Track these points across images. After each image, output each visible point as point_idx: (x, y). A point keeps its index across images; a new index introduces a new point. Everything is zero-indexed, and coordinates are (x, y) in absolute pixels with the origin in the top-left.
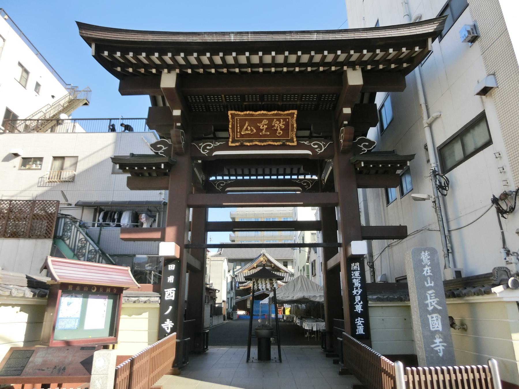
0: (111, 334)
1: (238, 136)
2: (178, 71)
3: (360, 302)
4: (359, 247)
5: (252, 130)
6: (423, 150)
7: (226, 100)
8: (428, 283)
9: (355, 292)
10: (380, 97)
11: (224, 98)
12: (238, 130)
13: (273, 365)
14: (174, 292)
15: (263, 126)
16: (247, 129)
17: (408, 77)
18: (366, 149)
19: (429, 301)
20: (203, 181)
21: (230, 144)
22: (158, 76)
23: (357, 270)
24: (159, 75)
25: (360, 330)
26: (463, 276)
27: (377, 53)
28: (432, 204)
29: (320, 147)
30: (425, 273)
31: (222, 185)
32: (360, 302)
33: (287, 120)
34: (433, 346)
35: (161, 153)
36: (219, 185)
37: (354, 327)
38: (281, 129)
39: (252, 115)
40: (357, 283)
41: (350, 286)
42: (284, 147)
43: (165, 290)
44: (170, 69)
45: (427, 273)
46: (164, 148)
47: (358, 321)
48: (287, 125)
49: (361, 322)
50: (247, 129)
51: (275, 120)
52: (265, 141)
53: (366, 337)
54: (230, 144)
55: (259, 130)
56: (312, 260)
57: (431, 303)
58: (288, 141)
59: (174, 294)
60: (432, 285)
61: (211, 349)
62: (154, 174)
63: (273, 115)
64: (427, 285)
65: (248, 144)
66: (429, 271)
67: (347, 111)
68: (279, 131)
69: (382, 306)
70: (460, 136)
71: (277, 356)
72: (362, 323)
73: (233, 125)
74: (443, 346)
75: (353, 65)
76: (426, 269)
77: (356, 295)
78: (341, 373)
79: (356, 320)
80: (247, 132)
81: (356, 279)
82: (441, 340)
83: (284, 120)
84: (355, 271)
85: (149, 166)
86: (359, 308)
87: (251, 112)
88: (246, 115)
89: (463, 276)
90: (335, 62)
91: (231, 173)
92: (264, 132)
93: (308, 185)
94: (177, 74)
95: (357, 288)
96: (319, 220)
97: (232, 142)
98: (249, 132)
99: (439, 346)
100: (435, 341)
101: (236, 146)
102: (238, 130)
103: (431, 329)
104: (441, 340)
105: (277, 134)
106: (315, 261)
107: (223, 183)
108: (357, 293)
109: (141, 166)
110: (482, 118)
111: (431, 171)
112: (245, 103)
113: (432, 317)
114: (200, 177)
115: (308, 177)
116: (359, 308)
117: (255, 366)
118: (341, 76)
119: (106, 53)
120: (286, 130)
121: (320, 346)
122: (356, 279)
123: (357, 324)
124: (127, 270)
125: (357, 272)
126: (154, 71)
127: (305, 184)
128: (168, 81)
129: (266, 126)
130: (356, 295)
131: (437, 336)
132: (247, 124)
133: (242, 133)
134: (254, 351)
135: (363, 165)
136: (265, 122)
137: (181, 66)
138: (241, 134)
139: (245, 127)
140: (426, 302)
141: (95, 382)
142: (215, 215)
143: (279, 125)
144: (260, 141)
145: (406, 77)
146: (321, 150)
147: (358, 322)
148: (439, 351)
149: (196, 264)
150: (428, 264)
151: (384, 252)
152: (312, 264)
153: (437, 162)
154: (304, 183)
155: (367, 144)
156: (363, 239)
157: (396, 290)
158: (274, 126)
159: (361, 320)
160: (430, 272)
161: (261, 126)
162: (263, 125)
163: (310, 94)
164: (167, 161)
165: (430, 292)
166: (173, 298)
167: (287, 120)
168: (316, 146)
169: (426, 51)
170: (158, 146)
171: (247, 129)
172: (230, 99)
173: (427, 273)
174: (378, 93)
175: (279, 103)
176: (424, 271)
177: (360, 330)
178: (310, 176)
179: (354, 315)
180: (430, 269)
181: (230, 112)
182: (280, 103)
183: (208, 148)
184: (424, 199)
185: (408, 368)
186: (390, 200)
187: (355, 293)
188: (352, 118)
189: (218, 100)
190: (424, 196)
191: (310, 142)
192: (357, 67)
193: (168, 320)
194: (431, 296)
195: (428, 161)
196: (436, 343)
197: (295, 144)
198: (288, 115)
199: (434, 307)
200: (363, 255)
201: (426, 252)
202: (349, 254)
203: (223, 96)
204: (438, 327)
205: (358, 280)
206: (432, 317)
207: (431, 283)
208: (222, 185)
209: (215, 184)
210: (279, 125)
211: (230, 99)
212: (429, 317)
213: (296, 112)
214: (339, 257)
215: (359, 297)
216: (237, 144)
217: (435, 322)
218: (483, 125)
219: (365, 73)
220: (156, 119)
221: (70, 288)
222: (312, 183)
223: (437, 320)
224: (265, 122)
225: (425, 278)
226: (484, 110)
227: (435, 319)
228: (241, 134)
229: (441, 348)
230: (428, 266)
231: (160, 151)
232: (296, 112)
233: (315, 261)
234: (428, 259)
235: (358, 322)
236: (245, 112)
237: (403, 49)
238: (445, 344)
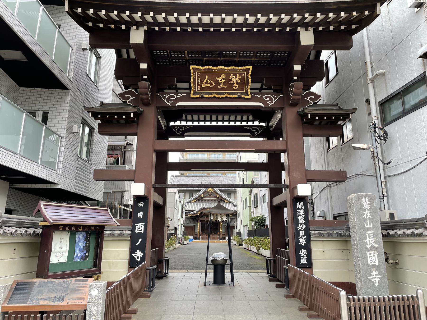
0: (95, 266)
1: (199, 89)
2: (146, 28)
3: (303, 236)
4: (303, 190)
5: (211, 84)
6: (365, 104)
7: (188, 55)
8: (367, 225)
9: (299, 227)
10: (325, 55)
11: (186, 54)
12: (199, 83)
13: (227, 288)
14: (143, 226)
15: (221, 80)
16: (206, 83)
17: (355, 37)
18: (312, 102)
19: (368, 240)
20: (164, 126)
21: (192, 96)
22: (127, 32)
23: (302, 209)
24: (128, 31)
25: (304, 260)
26: (396, 218)
27: (330, 16)
28: (371, 155)
29: (271, 100)
30: (365, 215)
31: (181, 130)
32: (303, 236)
33: (243, 75)
34: (370, 278)
35: (129, 102)
36: (178, 130)
37: (298, 257)
38: (237, 83)
39: (211, 70)
40: (301, 220)
41: (296, 222)
42: (239, 99)
43: (136, 225)
44: (139, 25)
45: (367, 216)
46: (131, 98)
47: (302, 252)
48: (242, 79)
49: (304, 253)
50: (207, 83)
51: (232, 75)
52: (223, 94)
53: (309, 265)
54: (192, 96)
55: (218, 84)
56: (255, 193)
57: (369, 241)
58: (242, 94)
59: (143, 228)
60: (371, 226)
61: (172, 274)
62: (123, 122)
63: (231, 70)
65: (207, 96)
66: (369, 214)
67: (297, 67)
68: (235, 85)
71: (230, 280)
72: (305, 254)
73: (194, 79)
74: (378, 278)
75: (306, 26)
76: (366, 213)
77: (300, 230)
78: (287, 297)
79: (300, 252)
80: (207, 85)
81: (301, 216)
83: (240, 74)
84: (300, 209)
85: (120, 115)
86: (303, 241)
87: (211, 67)
88: (206, 70)
89: (396, 218)
90: (290, 23)
91: (188, 119)
92: (221, 85)
93: (257, 131)
94: (145, 31)
95: (301, 224)
96: (265, 161)
97: (193, 94)
98: (209, 85)
99: (375, 278)
100: (372, 274)
101: (197, 98)
102: (199, 83)
103: (369, 263)
105: (234, 88)
106: (257, 194)
107: (182, 129)
108: (302, 228)
109: (112, 114)
111: (371, 124)
112: (205, 59)
114: (163, 123)
115: (256, 123)
116: (303, 241)
117: (212, 288)
118: (295, 35)
119: (79, 10)
120: (241, 84)
121: (266, 271)
122: (301, 216)
123: (301, 255)
124: (107, 210)
126: (124, 27)
127: (255, 130)
128: (137, 37)
129: (224, 80)
132: (207, 78)
133: (203, 86)
134: (211, 275)
135: (309, 117)
136: (223, 76)
137: (149, 24)
138: (201, 87)
139: (205, 81)
140: (366, 241)
141: (90, 309)
142: (174, 157)
143: (235, 79)
144: (218, 94)
145: (353, 36)
147: (302, 254)
148: (375, 282)
149: (160, 201)
150: (368, 208)
151: (323, 191)
152: (254, 196)
153: (377, 115)
154: (253, 129)
155: (313, 97)
156: (309, 181)
157: (340, 228)
158: (231, 80)
159: (304, 252)
160: (370, 216)
161: (220, 80)
162: (221, 79)
163: (264, 52)
164: (136, 111)
165: (369, 232)
166: (142, 232)
167: (243, 75)
168: (268, 99)
169: (374, 15)
170: (126, 96)
171: (206, 83)
172: (191, 55)
173: (367, 216)
174: (323, 51)
175: (236, 59)
176: (364, 214)
177: (304, 260)
178: (258, 122)
179: (298, 247)
180: (369, 213)
181: (192, 67)
182: (237, 59)
183: (172, 99)
184: (363, 149)
185: (351, 297)
186: (331, 146)
187: (300, 229)
188: (302, 75)
189: (181, 55)
190: (365, 146)
191: (263, 95)
192: (311, 29)
193: (138, 251)
194: (369, 236)
195: (370, 114)
196: (373, 275)
197: (249, 97)
198: (244, 70)
199: (372, 245)
200: (307, 196)
201: (367, 198)
202: (295, 195)
203: (186, 51)
204: (375, 262)
205: (302, 217)
206: (370, 254)
207: (370, 224)
208: (181, 130)
209: (175, 129)
210: (235, 79)
211: (191, 55)
212: (368, 253)
213: (251, 67)
214: (285, 196)
215: (303, 232)
216: (198, 96)
217: (373, 258)
219: (316, 33)
220: (125, 71)
221: (61, 228)
222: (260, 130)
223: (374, 256)
224: (223, 76)
225: (365, 220)
226: (425, 72)
227: (372, 255)
228: (201, 87)
229: (377, 279)
230: (368, 210)
231: (128, 101)
232: (251, 67)
233: (257, 194)
234: (368, 204)
235: (302, 254)
236: (206, 67)
237: (354, 12)
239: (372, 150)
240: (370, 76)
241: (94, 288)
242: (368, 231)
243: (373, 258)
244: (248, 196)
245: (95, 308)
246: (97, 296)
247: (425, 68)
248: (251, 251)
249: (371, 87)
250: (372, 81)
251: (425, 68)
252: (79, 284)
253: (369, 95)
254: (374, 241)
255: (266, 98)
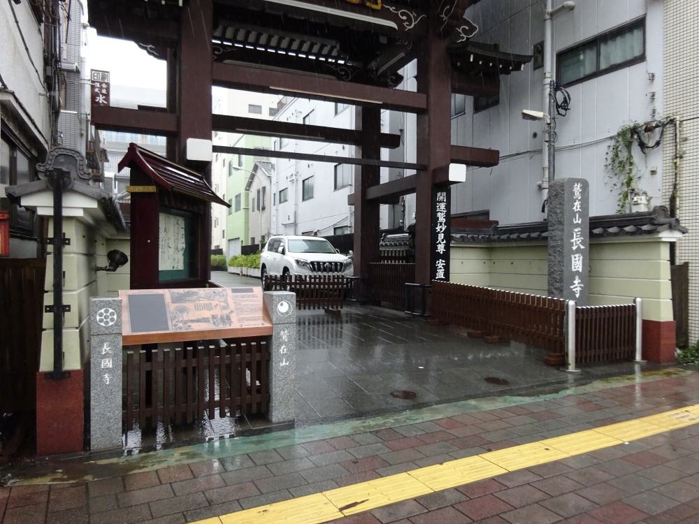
3: (443, 240)
9: (438, 228)
18: (465, 36)
19: (575, 239)
23: (443, 202)
29: (409, 20)
30: (575, 208)
32: (443, 240)
34: (572, 287)
45: (577, 208)
64: (575, 222)
66: (579, 206)
69: (462, 247)
70: (595, 43)
72: (443, 266)
76: (576, 204)
77: (439, 233)
81: (441, 212)
82: (580, 281)
84: (440, 202)
95: (441, 224)
99: (576, 287)
100: (575, 282)
104: (580, 281)
108: (441, 229)
110: (639, 24)
113: (575, 257)
116: (441, 249)
125: (442, 204)
130: (439, 233)
131: (577, 277)
140: (572, 241)
141: (279, 333)
146: (410, 25)
154: (341, 70)
155: (467, 28)
160: (580, 208)
165: (576, 230)
168: (404, 18)
173: (577, 208)
187: (439, 230)
190: (539, 114)
194: (577, 235)
197: (378, 7)
206: (575, 257)
212: (573, 256)
215: (443, 234)
218: (637, 34)
226: (646, 14)
229: (579, 289)
230: (579, 200)
238: (583, 285)
239: (549, 122)
240: (549, 9)
241: (282, 300)
242: (577, 227)
243: (577, 262)
244: (243, 191)
245: (286, 332)
246: (287, 313)
247: (646, 9)
248: (247, 276)
249: (548, 24)
250: (552, 14)
251: (646, 9)
252: (243, 297)
253: (543, 34)
254: (580, 241)
255: (402, 15)
